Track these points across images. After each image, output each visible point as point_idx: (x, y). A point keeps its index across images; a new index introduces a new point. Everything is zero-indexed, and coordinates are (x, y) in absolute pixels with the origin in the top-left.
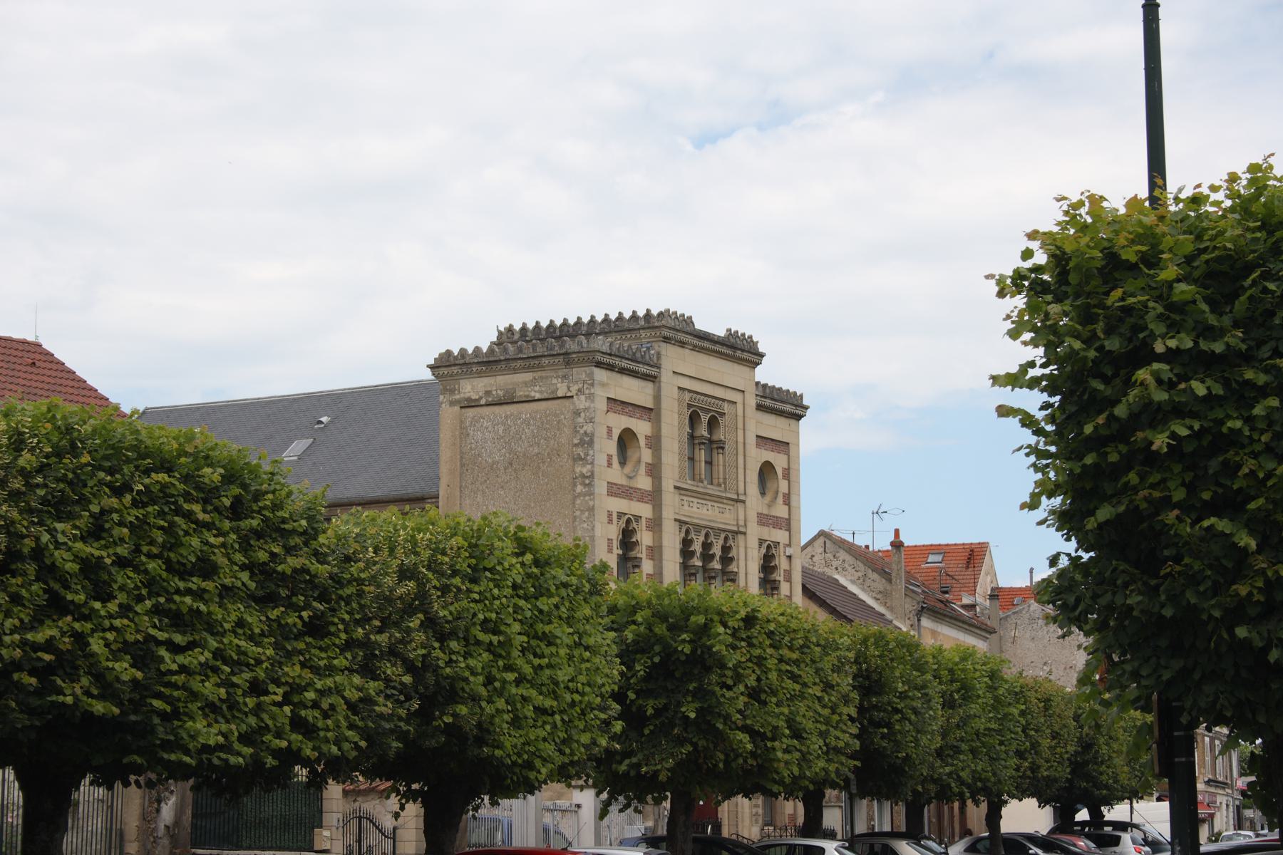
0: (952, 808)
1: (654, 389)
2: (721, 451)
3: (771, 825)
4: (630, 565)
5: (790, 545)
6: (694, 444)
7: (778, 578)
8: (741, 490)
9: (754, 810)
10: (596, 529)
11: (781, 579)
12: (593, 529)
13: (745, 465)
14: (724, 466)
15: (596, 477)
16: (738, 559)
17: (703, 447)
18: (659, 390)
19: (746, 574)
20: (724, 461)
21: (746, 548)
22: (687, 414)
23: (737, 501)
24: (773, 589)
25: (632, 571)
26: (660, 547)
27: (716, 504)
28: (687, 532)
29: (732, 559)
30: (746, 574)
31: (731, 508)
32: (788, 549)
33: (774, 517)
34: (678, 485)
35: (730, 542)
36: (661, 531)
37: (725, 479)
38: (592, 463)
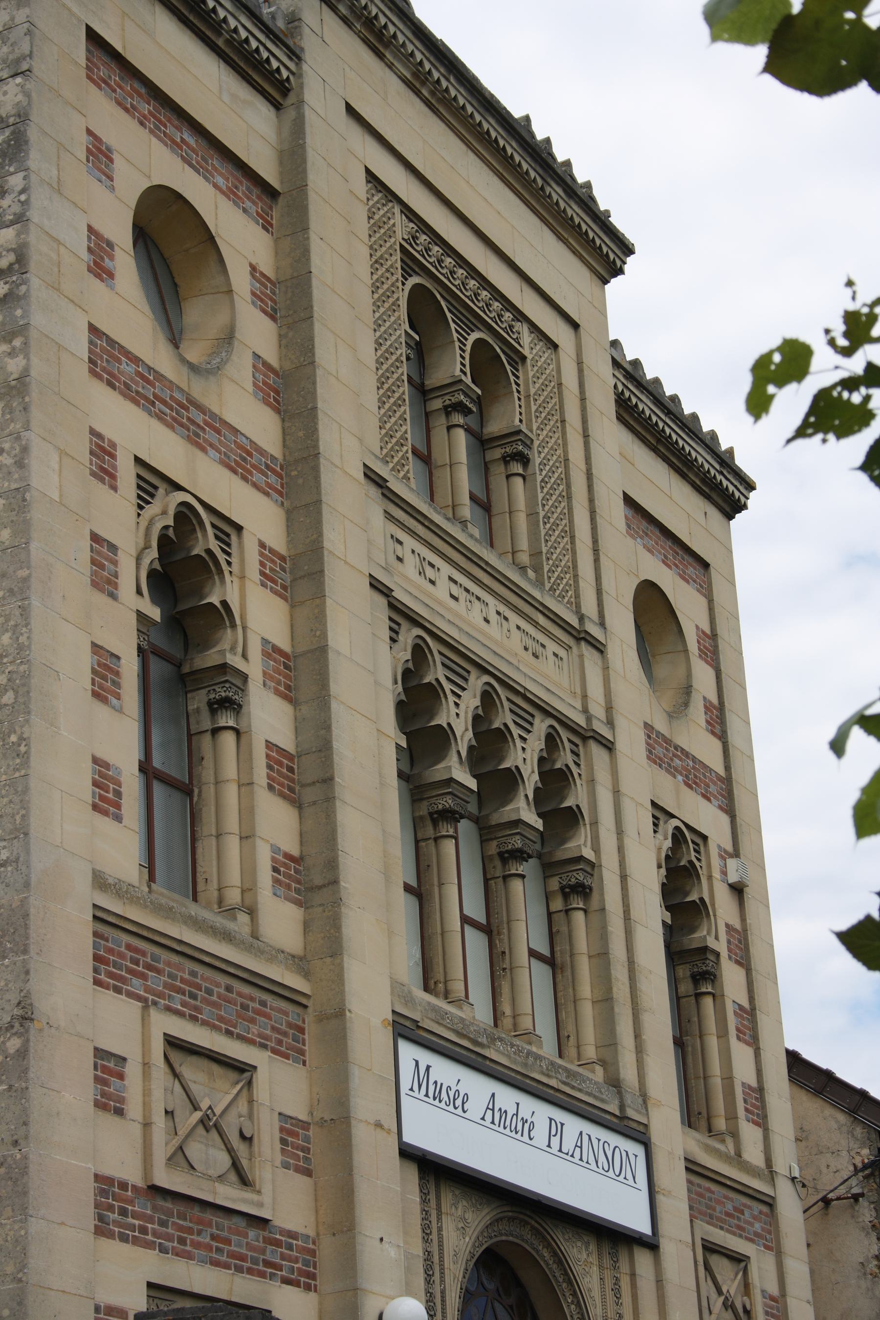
1: (279, 132)
2: (517, 468)
4: (199, 700)
5: (736, 854)
6: (427, 415)
7: (711, 943)
10: (34, 463)
11: (721, 947)
12: (20, 464)
14: (532, 515)
15: (32, 266)
16: (595, 823)
17: (458, 419)
18: (298, 130)
20: (531, 500)
21: (616, 793)
23: (582, 637)
25: (207, 724)
26: (320, 652)
27: (514, 619)
28: (419, 652)
29: (573, 817)
31: (562, 653)
32: (732, 863)
33: (687, 754)
34: (383, 471)
35: (565, 758)
36: (319, 595)
37: (536, 554)
38: (20, 219)
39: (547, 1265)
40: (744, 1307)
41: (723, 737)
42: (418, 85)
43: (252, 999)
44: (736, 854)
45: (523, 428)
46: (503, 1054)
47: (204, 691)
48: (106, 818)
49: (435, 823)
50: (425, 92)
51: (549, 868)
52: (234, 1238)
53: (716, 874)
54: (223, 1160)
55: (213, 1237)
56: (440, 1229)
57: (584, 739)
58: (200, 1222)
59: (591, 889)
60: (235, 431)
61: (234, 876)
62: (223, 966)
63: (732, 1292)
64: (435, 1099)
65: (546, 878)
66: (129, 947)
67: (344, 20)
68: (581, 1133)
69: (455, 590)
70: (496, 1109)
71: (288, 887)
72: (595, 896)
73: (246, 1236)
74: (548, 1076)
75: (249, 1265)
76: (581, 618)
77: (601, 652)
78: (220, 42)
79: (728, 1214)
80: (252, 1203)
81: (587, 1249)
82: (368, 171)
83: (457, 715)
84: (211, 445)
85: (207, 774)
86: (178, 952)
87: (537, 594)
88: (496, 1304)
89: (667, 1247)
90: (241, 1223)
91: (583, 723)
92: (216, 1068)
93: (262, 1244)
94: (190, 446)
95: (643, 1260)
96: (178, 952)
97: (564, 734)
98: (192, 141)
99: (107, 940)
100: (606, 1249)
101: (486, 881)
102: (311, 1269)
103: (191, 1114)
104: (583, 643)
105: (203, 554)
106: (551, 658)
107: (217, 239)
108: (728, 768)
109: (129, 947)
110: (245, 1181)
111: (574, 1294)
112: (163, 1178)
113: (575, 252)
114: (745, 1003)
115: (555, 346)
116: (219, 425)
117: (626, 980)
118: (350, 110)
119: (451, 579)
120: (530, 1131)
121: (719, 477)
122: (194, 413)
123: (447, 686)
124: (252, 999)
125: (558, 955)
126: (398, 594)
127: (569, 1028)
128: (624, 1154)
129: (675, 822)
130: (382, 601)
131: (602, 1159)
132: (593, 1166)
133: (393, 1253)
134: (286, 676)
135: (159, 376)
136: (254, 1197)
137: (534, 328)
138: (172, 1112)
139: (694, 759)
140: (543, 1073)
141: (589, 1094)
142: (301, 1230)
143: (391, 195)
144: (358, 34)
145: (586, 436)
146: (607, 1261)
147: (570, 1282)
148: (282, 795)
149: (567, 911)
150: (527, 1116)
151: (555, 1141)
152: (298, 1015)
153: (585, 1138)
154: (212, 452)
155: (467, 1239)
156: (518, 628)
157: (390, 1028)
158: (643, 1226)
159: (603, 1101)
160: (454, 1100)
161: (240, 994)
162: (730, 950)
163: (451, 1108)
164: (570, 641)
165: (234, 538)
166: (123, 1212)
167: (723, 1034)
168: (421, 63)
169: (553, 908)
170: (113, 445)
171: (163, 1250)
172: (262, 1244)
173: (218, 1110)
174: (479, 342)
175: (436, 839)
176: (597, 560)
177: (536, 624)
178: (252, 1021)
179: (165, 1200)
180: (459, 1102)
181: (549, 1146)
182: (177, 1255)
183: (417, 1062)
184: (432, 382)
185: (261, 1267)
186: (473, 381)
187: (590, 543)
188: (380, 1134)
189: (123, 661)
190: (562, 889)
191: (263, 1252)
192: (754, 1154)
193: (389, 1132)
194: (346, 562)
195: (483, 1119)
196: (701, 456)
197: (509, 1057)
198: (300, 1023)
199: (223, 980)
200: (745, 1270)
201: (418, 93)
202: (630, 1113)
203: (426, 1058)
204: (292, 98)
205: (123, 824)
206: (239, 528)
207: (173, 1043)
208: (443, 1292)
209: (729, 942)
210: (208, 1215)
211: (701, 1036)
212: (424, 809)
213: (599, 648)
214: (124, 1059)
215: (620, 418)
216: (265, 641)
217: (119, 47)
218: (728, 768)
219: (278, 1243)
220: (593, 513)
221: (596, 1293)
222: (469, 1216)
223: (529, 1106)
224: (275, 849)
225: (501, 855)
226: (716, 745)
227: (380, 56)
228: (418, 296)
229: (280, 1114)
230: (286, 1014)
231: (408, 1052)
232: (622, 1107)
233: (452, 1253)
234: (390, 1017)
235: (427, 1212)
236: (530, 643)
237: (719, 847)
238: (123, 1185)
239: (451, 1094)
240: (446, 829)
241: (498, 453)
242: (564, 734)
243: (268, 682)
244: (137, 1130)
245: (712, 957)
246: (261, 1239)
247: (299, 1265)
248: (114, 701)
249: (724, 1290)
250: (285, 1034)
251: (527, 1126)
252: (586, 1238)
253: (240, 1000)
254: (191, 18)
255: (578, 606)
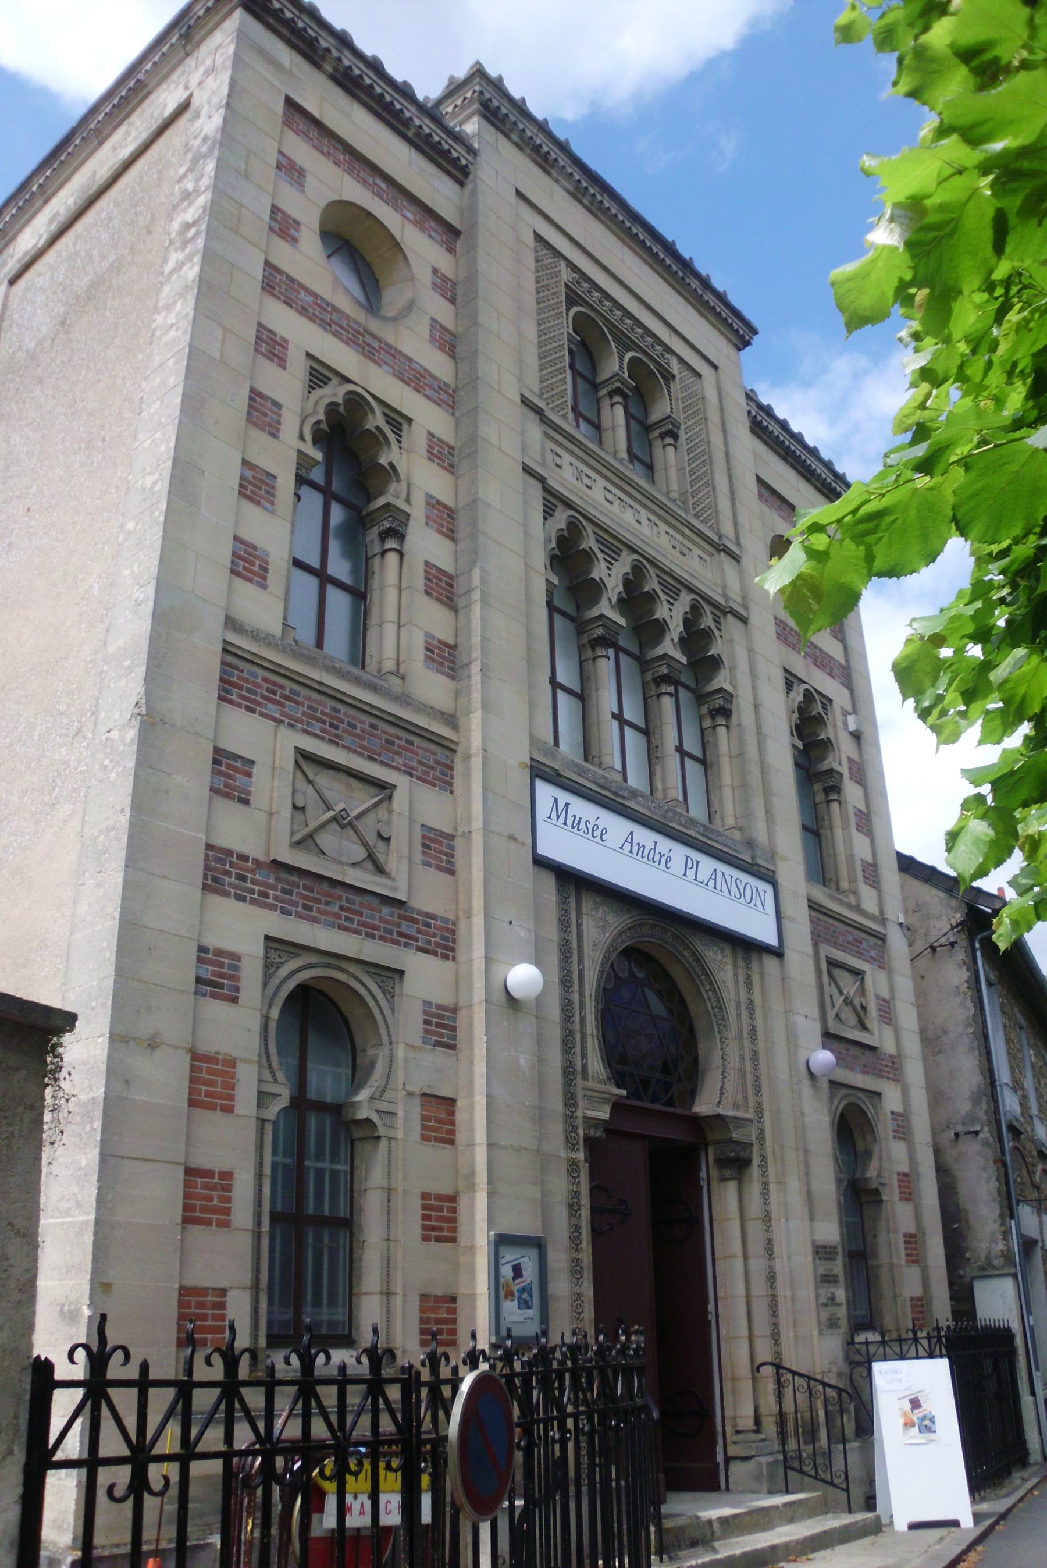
0: (724, 1521)
2: (669, 440)
3: (869, 1326)
5: (855, 712)
7: (835, 766)
8: (727, 529)
9: (825, 1292)
11: (844, 770)
13: (732, 493)
16: (733, 669)
19: (756, 706)
22: (564, 330)
24: (828, 790)
30: (756, 706)
31: (706, 557)
32: (851, 719)
33: (816, 647)
39: (688, 962)
40: (862, 1005)
41: (843, 641)
42: (580, 196)
43: (398, 738)
44: (855, 712)
45: (674, 416)
46: (644, 806)
47: (376, 528)
48: (250, 584)
49: (593, 648)
50: (585, 201)
51: (701, 698)
52: (365, 911)
53: (840, 724)
54: (360, 853)
55: (342, 908)
56: (579, 926)
57: (725, 613)
58: (328, 895)
59: (731, 712)
60: (411, 360)
61: (390, 651)
62: (367, 708)
63: (851, 994)
64: (573, 827)
65: (699, 705)
66: (265, 680)
67: (517, 145)
68: (715, 870)
69: (610, 497)
70: (635, 843)
71: (442, 664)
72: (734, 717)
73: (380, 911)
74: (685, 827)
75: (382, 933)
76: (720, 536)
77: (738, 561)
78: (410, 134)
79: (848, 943)
80: (386, 886)
81: (722, 953)
82: (535, 233)
83: (610, 575)
84: (386, 363)
85: (375, 583)
86: (320, 692)
87: (683, 514)
88: (648, 991)
89: (790, 955)
90: (375, 902)
91: (723, 603)
92: (354, 783)
93: (396, 919)
94: (363, 358)
95: (770, 963)
96: (320, 692)
97: (707, 609)
98: (384, 186)
99: (242, 671)
100: (740, 953)
101: (645, 700)
102: (450, 944)
103: (325, 813)
104: (722, 553)
105: (374, 430)
106: (696, 558)
107: (403, 247)
108: (847, 660)
109: (265, 680)
110: (380, 870)
111: (711, 984)
112: (288, 856)
113: (714, 326)
114: (863, 808)
115: (700, 376)
116: (393, 352)
117: (759, 773)
118: (518, 193)
119: (605, 488)
120: (667, 863)
121: (834, 485)
122: (368, 339)
123: (600, 555)
124: (398, 738)
125: (708, 758)
126: (551, 482)
127: (716, 806)
128: (755, 890)
129: (805, 686)
130: (539, 485)
131: (734, 889)
132: (726, 893)
133: (523, 934)
134: (448, 523)
135: (335, 309)
136: (389, 882)
137: (681, 360)
138: (303, 809)
139: (821, 650)
140: (681, 825)
141: (725, 845)
142: (440, 913)
143: (557, 254)
144: (529, 156)
145: (724, 431)
146: (741, 963)
147: (707, 975)
148: (439, 600)
149: (714, 727)
150: (664, 851)
151: (691, 873)
152: (447, 756)
153: (719, 875)
154: (385, 367)
155: (607, 935)
156: (667, 533)
157: (529, 770)
158: (772, 940)
159: (736, 851)
160: (593, 831)
161: (384, 732)
162: (850, 773)
163: (590, 836)
164: (714, 552)
165: (405, 426)
166: (242, 878)
167: (846, 827)
168: (579, 181)
169: (704, 726)
170: (286, 341)
171: (284, 911)
172: (396, 919)
173: (353, 814)
174: (632, 360)
175: (594, 659)
176: (733, 505)
177: (683, 534)
178: (398, 754)
179: (290, 874)
180: (597, 833)
181: (685, 875)
182: (301, 917)
183: (556, 800)
184: (599, 380)
185: (395, 937)
186: (630, 377)
187: (728, 493)
188: (513, 845)
189: (279, 480)
190: (710, 712)
191: (399, 925)
192: (870, 904)
193: (523, 844)
194: (499, 449)
195: (621, 848)
196: (820, 470)
197: (649, 809)
198: (448, 762)
199: (369, 720)
200: (862, 980)
201: (580, 202)
202: (760, 861)
203: (564, 797)
204: (471, 177)
205: (269, 590)
206: (410, 421)
207: (304, 756)
208: (581, 972)
209: (850, 768)
210: (338, 891)
211: (831, 829)
212: (585, 639)
213: (736, 559)
214: (253, 762)
215: (752, 430)
216: (429, 496)
217: (316, 114)
218: (847, 660)
219: (415, 921)
220: (730, 477)
221: (730, 983)
222: (610, 918)
223: (665, 845)
224: (429, 635)
225: (654, 680)
226: (839, 646)
227: (548, 174)
228: (581, 324)
229: (423, 825)
230: (435, 754)
231: (546, 793)
232: (753, 858)
233: (591, 943)
234: (528, 762)
235: (566, 911)
236: (677, 545)
237: (842, 708)
238: (244, 858)
239: (590, 827)
240: (600, 651)
241: (656, 433)
242: (707, 609)
243: (431, 523)
244: (262, 817)
245: (837, 777)
246: (396, 915)
247: (438, 939)
248: (267, 505)
249: (845, 992)
250: (432, 768)
251: (664, 859)
252: (721, 945)
253: (384, 737)
254: (384, 114)
255: (718, 529)
